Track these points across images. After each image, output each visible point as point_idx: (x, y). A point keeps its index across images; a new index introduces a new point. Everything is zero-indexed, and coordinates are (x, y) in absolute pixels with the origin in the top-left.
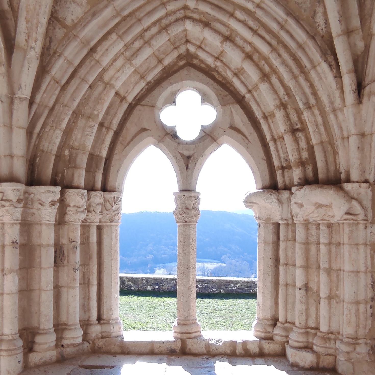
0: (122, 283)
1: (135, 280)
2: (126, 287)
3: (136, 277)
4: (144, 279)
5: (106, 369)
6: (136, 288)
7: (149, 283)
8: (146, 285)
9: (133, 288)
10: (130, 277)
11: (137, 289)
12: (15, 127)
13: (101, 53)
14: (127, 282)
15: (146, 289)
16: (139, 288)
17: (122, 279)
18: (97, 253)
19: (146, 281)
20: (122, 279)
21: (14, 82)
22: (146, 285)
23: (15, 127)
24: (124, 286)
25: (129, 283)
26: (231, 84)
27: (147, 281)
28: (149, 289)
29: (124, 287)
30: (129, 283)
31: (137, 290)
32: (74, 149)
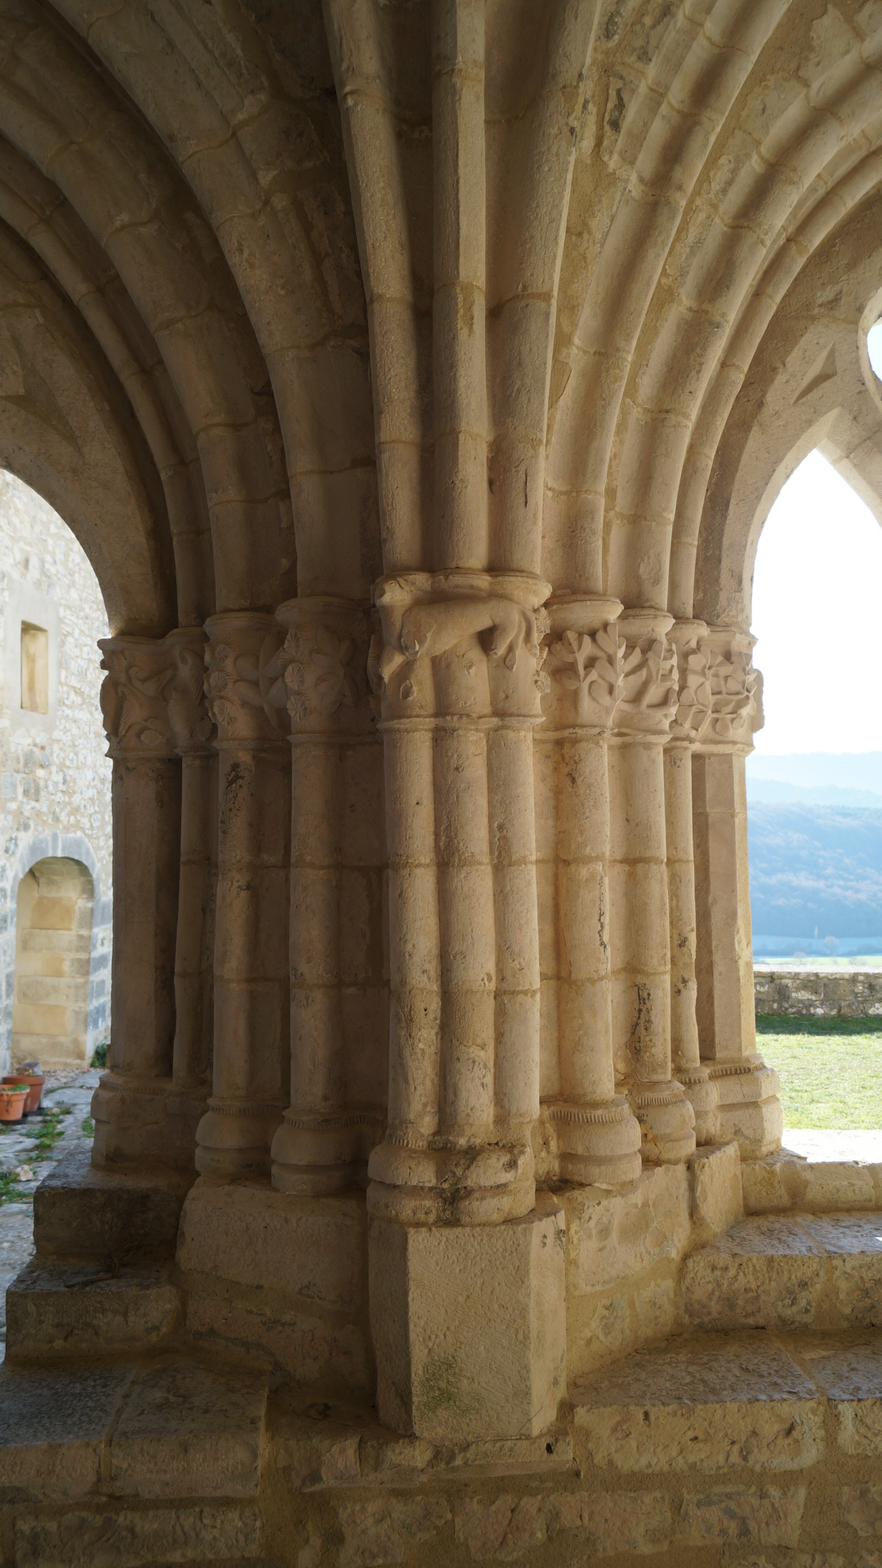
0: (779, 993)
1: (825, 985)
2: (792, 1006)
3: (832, 974)
4: (861, 978)
5: (236, 607)
6: (831, 1009)
7: (877, 991)
8: (865, 1001)
9: (820, 1011)
10: (808, 975)
11: (834, 1012)
12: (65, 776)
13: (690, 186)
14: (796, 992)
15: (866, 1014)
16: (839, 1011)
17: (777, 981)
18: (453, 434)
19: (866, 986)
20: (777, 981)
21: (458, 1059)
22: (865, 1001)
23: (65, 776)
24: (786, 1006)
25: (804, 995)
26: (830, 163)
27: (871, 987)
28: (877, 1012)
29: (787, 1009)
30: (804, 995)
31: (833, 1018)
32: (607, 591)
